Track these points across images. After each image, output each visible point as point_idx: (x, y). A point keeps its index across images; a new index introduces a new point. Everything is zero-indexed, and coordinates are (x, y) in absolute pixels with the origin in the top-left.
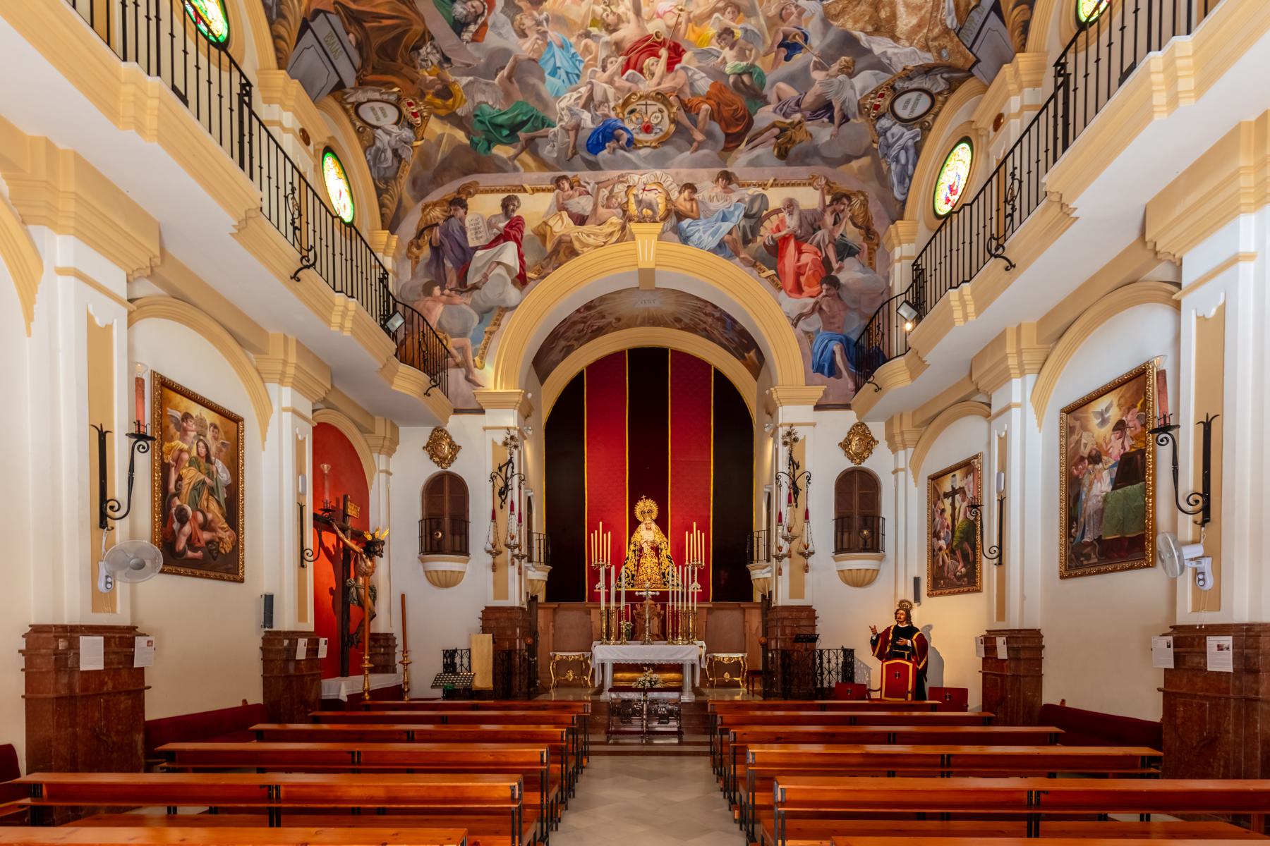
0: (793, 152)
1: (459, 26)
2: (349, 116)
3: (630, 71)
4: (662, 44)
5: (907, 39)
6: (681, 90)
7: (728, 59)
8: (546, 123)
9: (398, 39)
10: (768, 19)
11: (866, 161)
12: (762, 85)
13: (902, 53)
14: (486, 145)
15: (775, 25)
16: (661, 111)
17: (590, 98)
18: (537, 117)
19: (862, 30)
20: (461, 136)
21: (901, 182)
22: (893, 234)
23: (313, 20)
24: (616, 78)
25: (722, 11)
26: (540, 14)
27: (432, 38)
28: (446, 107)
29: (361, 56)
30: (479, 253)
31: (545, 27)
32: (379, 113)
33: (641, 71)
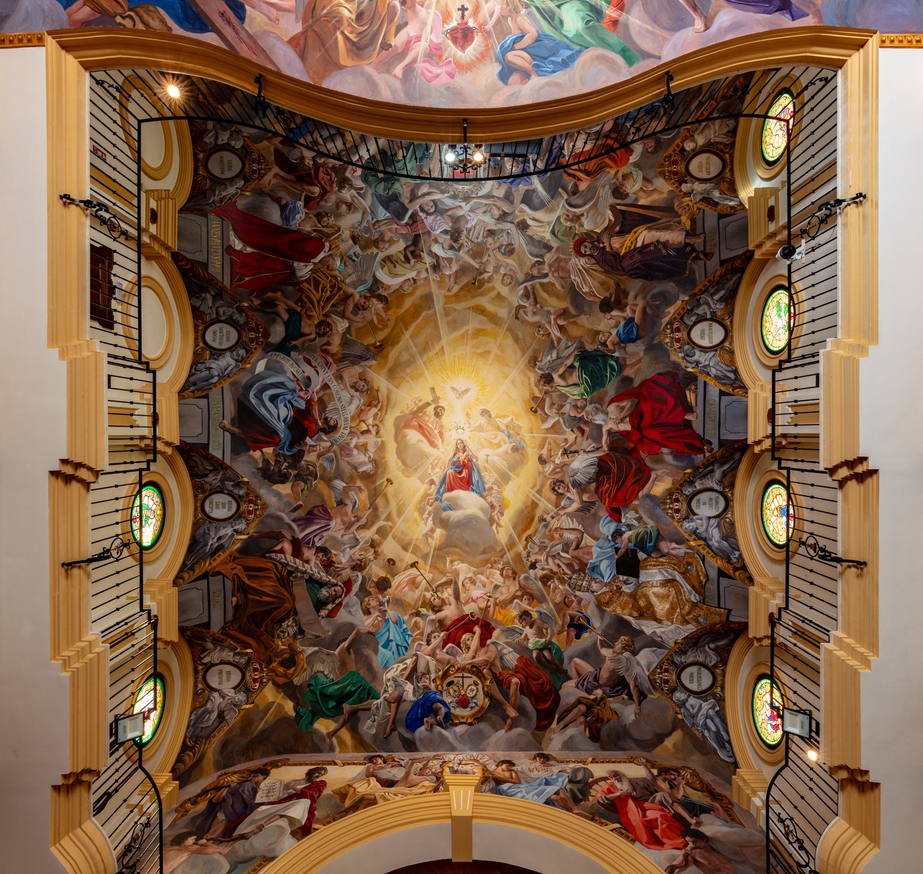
0: (604, 731)
1: (319, 605)
2: (196, 678)
3: (450, 645)
4: (476, 622)
5: (668, 619)
7: (529, 636)
9: (269, 613)
10: (555, 605)
11: (677, 735)
12: (562, 660)
13: (672, 632)
14: (310, 718)
16: (476, 684)
17: (414, 669)
18: (364, 688)
19: (630, 615)
20: (289, 707)
21: (722, 746)
22: (741, 784)
23: (213, 576)
24: (438, 651)
25: (521, 598)
27: (296, 614)
28: (286, 676)
29: (235, 614)
31: (386, 607)
32: (224, 677)
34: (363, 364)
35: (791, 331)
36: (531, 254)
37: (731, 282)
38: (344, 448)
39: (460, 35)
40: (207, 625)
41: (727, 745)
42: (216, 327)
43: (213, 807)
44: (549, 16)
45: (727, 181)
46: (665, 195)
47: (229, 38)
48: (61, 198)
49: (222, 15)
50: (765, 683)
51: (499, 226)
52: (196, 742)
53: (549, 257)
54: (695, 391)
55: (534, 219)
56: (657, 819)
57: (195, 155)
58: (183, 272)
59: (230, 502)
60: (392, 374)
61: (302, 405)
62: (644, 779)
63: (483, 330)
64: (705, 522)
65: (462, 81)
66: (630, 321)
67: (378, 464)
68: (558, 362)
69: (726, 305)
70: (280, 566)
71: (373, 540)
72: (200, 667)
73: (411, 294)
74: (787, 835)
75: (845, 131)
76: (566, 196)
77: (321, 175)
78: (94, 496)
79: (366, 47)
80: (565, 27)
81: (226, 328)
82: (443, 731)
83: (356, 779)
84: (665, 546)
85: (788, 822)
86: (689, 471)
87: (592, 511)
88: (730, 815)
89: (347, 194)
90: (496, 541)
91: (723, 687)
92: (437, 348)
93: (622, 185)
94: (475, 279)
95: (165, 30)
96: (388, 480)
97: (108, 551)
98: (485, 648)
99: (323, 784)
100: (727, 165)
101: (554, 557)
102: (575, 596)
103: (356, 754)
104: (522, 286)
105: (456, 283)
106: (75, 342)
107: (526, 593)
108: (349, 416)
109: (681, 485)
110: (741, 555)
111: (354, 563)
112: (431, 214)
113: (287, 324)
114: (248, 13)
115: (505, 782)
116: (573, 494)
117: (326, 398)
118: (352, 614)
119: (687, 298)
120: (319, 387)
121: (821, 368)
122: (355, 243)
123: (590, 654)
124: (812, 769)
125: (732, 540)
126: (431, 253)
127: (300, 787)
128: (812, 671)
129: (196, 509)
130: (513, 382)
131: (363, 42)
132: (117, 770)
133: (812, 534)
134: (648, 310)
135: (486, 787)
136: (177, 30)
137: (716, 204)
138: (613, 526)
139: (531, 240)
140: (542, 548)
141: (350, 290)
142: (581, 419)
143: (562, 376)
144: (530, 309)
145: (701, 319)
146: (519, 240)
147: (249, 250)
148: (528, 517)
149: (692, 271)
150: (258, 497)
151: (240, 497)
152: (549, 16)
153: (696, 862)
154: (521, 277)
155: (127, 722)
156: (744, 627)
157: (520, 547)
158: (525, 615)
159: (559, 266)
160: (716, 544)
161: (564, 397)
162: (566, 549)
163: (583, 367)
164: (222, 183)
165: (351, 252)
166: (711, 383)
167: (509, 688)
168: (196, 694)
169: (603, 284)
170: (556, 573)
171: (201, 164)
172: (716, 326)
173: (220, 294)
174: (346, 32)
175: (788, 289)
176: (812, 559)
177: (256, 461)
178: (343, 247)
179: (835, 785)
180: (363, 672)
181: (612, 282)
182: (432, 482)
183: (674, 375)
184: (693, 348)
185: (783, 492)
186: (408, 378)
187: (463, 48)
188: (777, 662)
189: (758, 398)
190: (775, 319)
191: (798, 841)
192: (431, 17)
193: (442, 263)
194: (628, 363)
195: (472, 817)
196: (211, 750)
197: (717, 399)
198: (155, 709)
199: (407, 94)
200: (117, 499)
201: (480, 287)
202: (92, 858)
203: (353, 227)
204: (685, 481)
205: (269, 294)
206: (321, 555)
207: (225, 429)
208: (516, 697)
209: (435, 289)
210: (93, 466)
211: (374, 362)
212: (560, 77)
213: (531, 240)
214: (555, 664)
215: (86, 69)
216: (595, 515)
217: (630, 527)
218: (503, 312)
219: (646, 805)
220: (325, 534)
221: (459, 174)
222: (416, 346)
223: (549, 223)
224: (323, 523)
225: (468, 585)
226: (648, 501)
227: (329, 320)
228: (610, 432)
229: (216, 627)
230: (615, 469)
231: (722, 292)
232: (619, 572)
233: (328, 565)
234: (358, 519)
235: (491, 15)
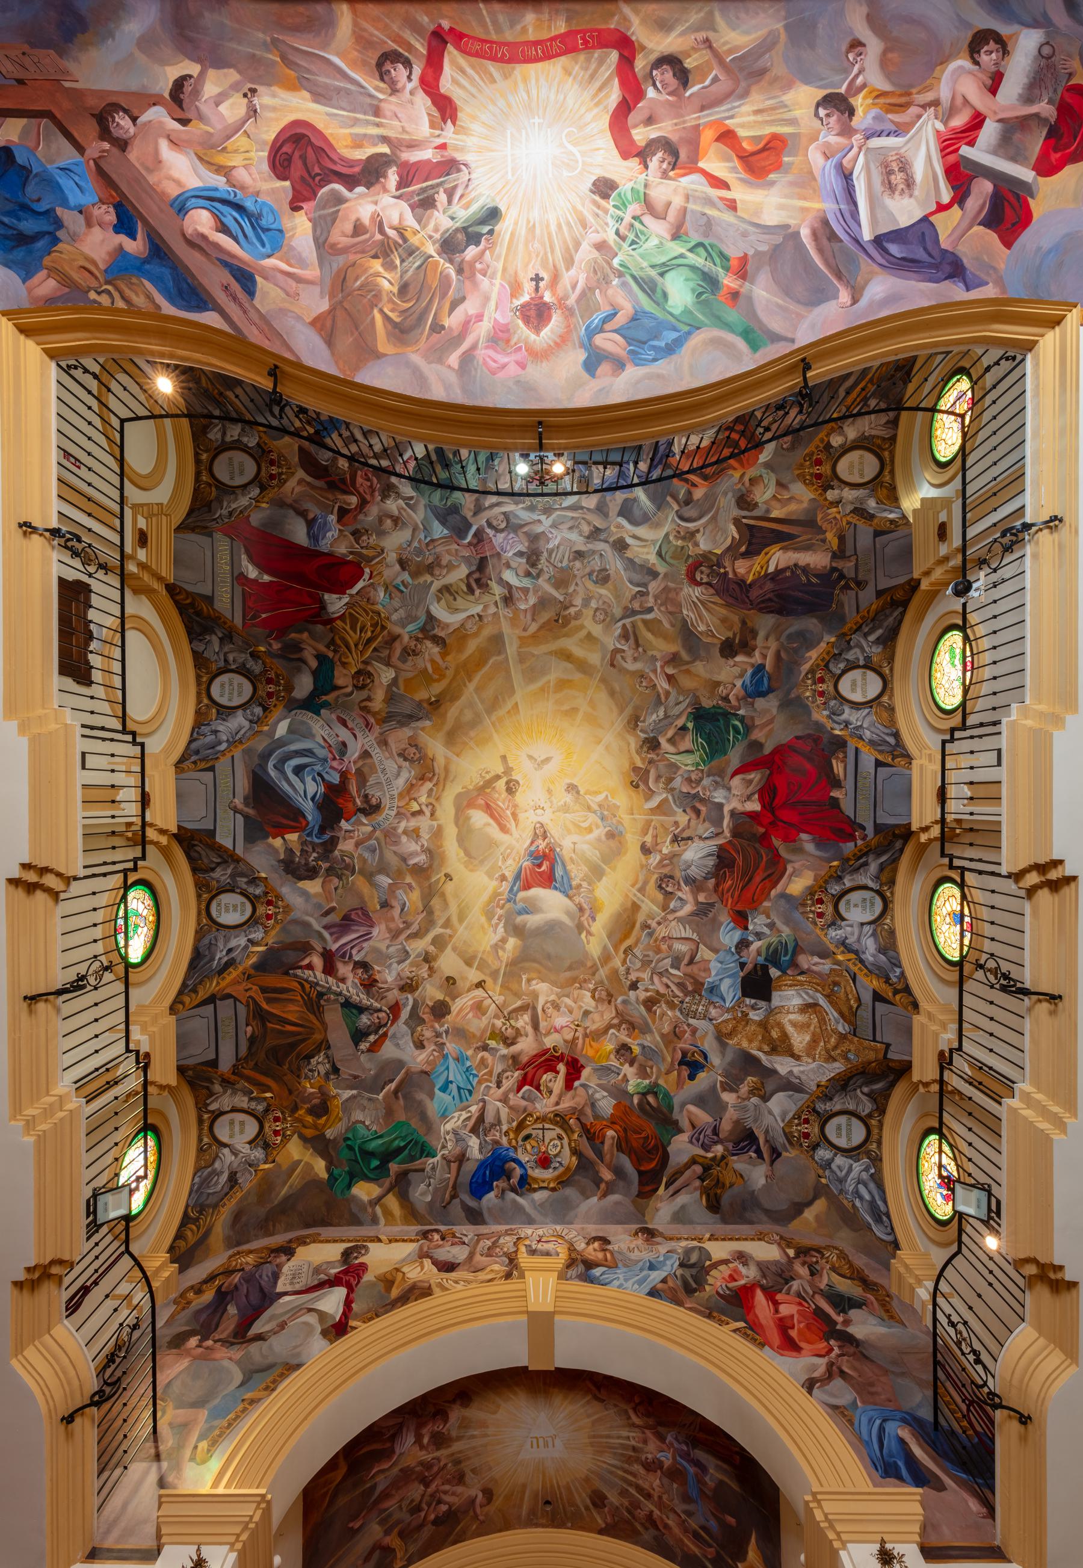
0: (725, 1200)
1: (358, 1036)
3: (526, 1088)
4: (560, 1059)
5: (808, 1055)
6: (582, 1112)
7: (629, 1076)
8: (426, 1151)
9: (293, 1046)
10: (662, 1036)
11: (820, 1205)
12: (671, 1108)
13: (814, 1071)
14: (347, 1179)
15: (670, 1042)
16: (560, 1138)
17: (481, 1119)
18: (416, 1143)
19: (760, 1049)
20: (320, 1166)
21: (878, 1220)
22: (902, 1270)
24: (511, 1096)
25: (618, 1027)
26: (442, 1026)
27: (329, 1047)
28: (315, 1126)
29: (249, 1049)
30: (287, 1298)
32: (237, 1128)
33: (538, 1088)
34: (414, 725)
35: (966, 691)
36: (631, 582)
37: (891, 619)
38: (390, 834)
39: (533, 313)
40: (214, 1063)
41: (885, 1218)
42: (224, 678)
43: (222, 1297)
44: (650, 287)
45: (885, 486)
46: (805, 505)
47: (235, 319)
48: (20, 526)
49: (226, 288)
50: (933, 1138)
51: (590, 546)
52: (200, 1213)
53: (654, 587)
54: (844, 761)
55: (635, 537)
56: (792, 1316)
57: (197, 455)
58: (181, 608)
59: (243, 904)
60: (451, 738)
61: (335, 779)
62: (776, 1263)
63: (569, 681)
64: (856, 931)
65: (535, 372)
66: (760, 669)
67: (434, 854)
68: (666, 722)
69: (885, 648)
70: (307, 986)
71: (427, 953)
72: (206, 1116)
73: (476, 634)
74: (958, 1344)
75: (1036, 434)
76: (676, 507)
77: (359, 480)
78: (65, 907)
79: (412, 329)
80: (670, 302)
81: (238, 679)
82: (518, 1198)
83: (405, 1261)
84: (804, 961)
85: (960, 1327)
86: (835, 863)
87: (711, 915)
88: (887, 1311)
89: (393, 505)
90: (586, 954)
91: (879, 1143)
92: (509, 705)
93: (749, 492)
94: (558, 615)
95: (152, 309)
96: (447, 876)
97: (82, 978)
98: (571, 1093)
99: (363, 1267)
100: (886, 465)
101: (661, 974)
102: (689, 1025)
103: (406, 1228)
104: (620, 624)
105: (533, 620)
106: (40, 712)
107: (625, 1021)
108: (395, 793)
109: (826, 882)
110: (903, 973)
111: (402, 983)
112: (502, 531)
113: (315, 674)
114: (259, 285)
115: (598, 1265)
116: (685, 893)
117: (366, 770)
118: (400, 1048)
119: (833, 639)
120: (357, 755)
121: (1004, 742)
122: (403, 569)
123: (707, 1100)
124: (991, 1259)
125: (891, 953)
126: (501, 582)
127: (334, 1271)
128: (992, 1126)
129: (199, 913)
130: (607, 748)
131: (408, 323)
132: (97, 1257)
133: (992, 955)
134: (783, 655)
135: (573, 1272)
136: (168, 309)
137: (872, 517)
138: (737, 935)
139: (631, 563)
140: (646, 963)
141: (397, 630)
142: (696, 796)
143: (671, 741)
144: (629, 654)
145: (852, 666)
146: (615, 565)
147: (266, 578)
148: (626, 924)
149: (841, 605)
150: (279, 897)
151: (256, 897)
152: (650, 287)
153: (842, 1374)
154: (618, 612)
155: (109, 1198)
156: (905, 1068)
157: (617, 962)
158: (623, 1050)
159: (667, 598)
160: (871, 959)
161: (674, 767)
162: (676, 963)
163: (698, 729)
164: (231, 491)
165: (398, 581)
166: (865, 749)
167: (603, 1143)
168: (201, 1150)
169: (724, 620)
170: (663, 995)
171: (204, 467)
172: (871, 675)
173: (228, 637)
174: (386, 310)
175: (963, 628)
176: (992, 987)
177: (276, 851)
178: (388, 573)
179: (1021, 1282)
180: (415, 1123)
181: (735, 619)
182: (503, 878)
183: (817, 740)
184: (841, 704)
185: (957, 892)
186: (472, 744)
187: (537, 330)
188: (946, 1117)
189: (924, 772)
190: (947, 667)
191: (974, 1352)
192: (496, 289)
193: (516, 595)
194: (757, 723)
195: (554, 1313)
196: (220, 1222)
197: (872, 771)
198: (145, 1177)
199: (465, 390)
200: (95, 909)
201: (564, 625)
202: (64, 1373)
203: (400, 548)
204: (831, 877)
205: (293, 635)
206: (360, 971)
207: (236, 811)
208: (612, 1155)
209: (506, 629)
210: (63, 871)
211: (428, 723)
212: (663, 366)
213: (631, 563)
214: (662, 1112)
215: (52, 357)
216: (714, 920)
217: (759, 936)
218: (594, 658)
219: (779, 1297)
220: (365, 945)
221: (533, 487)
222: (482, 701)
223: (654, 542)
224: (363, 930)
225: (550, 1011)
226: (783, 902)
227: (369, 668)
228: (733, 813)
229: (226, 1063)
230: (740, 861)
231: (879, 632)
232: (745, 994)
233: (370, 985)
234: (408, 925)
235: (574, 287)
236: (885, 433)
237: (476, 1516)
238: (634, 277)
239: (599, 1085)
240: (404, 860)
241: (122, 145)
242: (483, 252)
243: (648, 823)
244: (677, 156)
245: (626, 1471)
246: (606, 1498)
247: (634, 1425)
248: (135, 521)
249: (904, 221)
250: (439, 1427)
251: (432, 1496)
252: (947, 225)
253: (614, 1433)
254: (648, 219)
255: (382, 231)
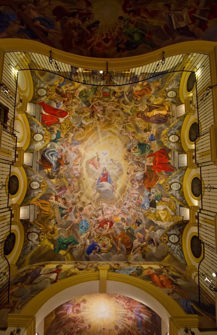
0: (146, 255)
3: (100, 228)
4: (108, 221)
5: (165, 221)
9: (47, 217)
10: (132, 216)
11: (169, 256)
12: (134, 233)
13: (166, 224)
16: (108, 240)
17: (90, 235)
18: (75, 241)
20: (52, 246)
21: (182, 259)
24: (97, 230)
27: (55, 218)
29: (37, 217)
30: (42, 275)
33: (103, 228)
44: (131, 36)
46: (161, 102)
51: (116, 109)
53: (129, 118)
54: (171, 154)
57: (34, 90)
61: (60, 157)
62: (159, 269)
64: (175, 192)
66: (152, 135)
67: (81, 174)
72: (26, 233)
76: (134, 102)
82: (98, 255)
83: (71, 268)
84: (164, 199)
89: (74, 100)
91: (182, 241)
92: (98, 141)
93: (149, 99)
96: (84, 179)
99: (61, 269)
101: (131, 202)
107: (123, 212)
110: (186, 201)
113: (56, 134)
115: (117, 269)
116: (137, 183)
117: (67, 155)
122: (76, 113)
126: (97, 116)
127: (54, 270)
130: (119, 151)
135: (111, 270)
138: (148, 193)
139: (125, 113)
142: (139, 162)
143: (133, 150)
145: (172, 134)
147: (47, 114)
149: (169, 121)
151: (41, 183)
153: (176, 292)
154: (122, 122)
157: (121, 199)
158: (123, 219)
161: (134, 155)
162: (135, 200)
163: (139, 147)
164: (41, 97)
168: (25, 241)
169: (144, 125)
170: (132, 207)
177: (46, 172)
180: (75, 236)
182: (96, 179)
187: (107, 43)
193: (100, 119)
194: (152, 146)
201: (111, 125)
205: (52, 126)
206: (63, 200)
213: (125, 113)
216: (143, 189)
217: (153, 193)
218: (117, 132)
220: (65, 194)
223: (130, 108)
224: (64, 191)
225: (106, 210)
226: (158, 186)
227: (68, 134)
232: (150, 206)
233: (65, 203)
234: (74, 190)
236: (177, 88)
237: (87, 331)
238: (127, 34)
239: (117, 228)
240: (74, 175)
241: (23, 10)
242: (96, 29)
243: (128, 168)
244: (136, 13)
245: (123, 320)
246: (118, 327)
247: (125, 308)
248: (20, 97)
249: (182, 26)
250: (78, 308)
251: (76, 326)
252: (191, 27)
253: (120, 310)
254: (130, 24)
255: (75, 25)
